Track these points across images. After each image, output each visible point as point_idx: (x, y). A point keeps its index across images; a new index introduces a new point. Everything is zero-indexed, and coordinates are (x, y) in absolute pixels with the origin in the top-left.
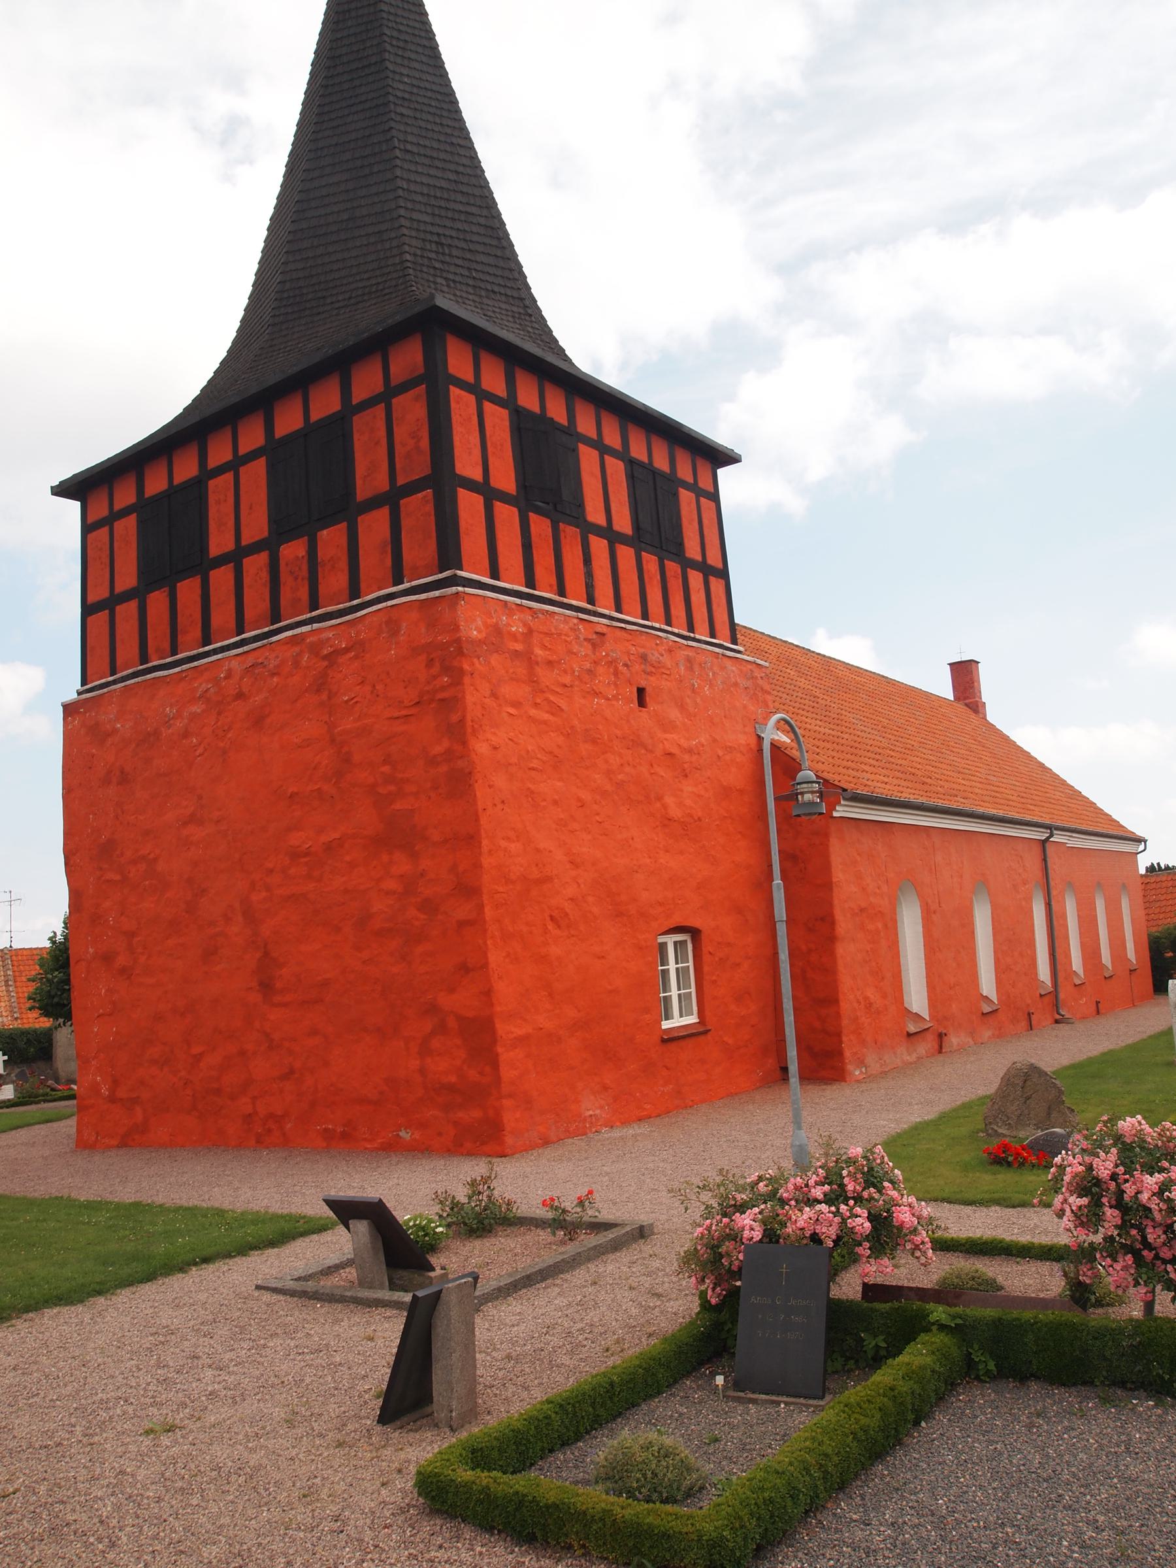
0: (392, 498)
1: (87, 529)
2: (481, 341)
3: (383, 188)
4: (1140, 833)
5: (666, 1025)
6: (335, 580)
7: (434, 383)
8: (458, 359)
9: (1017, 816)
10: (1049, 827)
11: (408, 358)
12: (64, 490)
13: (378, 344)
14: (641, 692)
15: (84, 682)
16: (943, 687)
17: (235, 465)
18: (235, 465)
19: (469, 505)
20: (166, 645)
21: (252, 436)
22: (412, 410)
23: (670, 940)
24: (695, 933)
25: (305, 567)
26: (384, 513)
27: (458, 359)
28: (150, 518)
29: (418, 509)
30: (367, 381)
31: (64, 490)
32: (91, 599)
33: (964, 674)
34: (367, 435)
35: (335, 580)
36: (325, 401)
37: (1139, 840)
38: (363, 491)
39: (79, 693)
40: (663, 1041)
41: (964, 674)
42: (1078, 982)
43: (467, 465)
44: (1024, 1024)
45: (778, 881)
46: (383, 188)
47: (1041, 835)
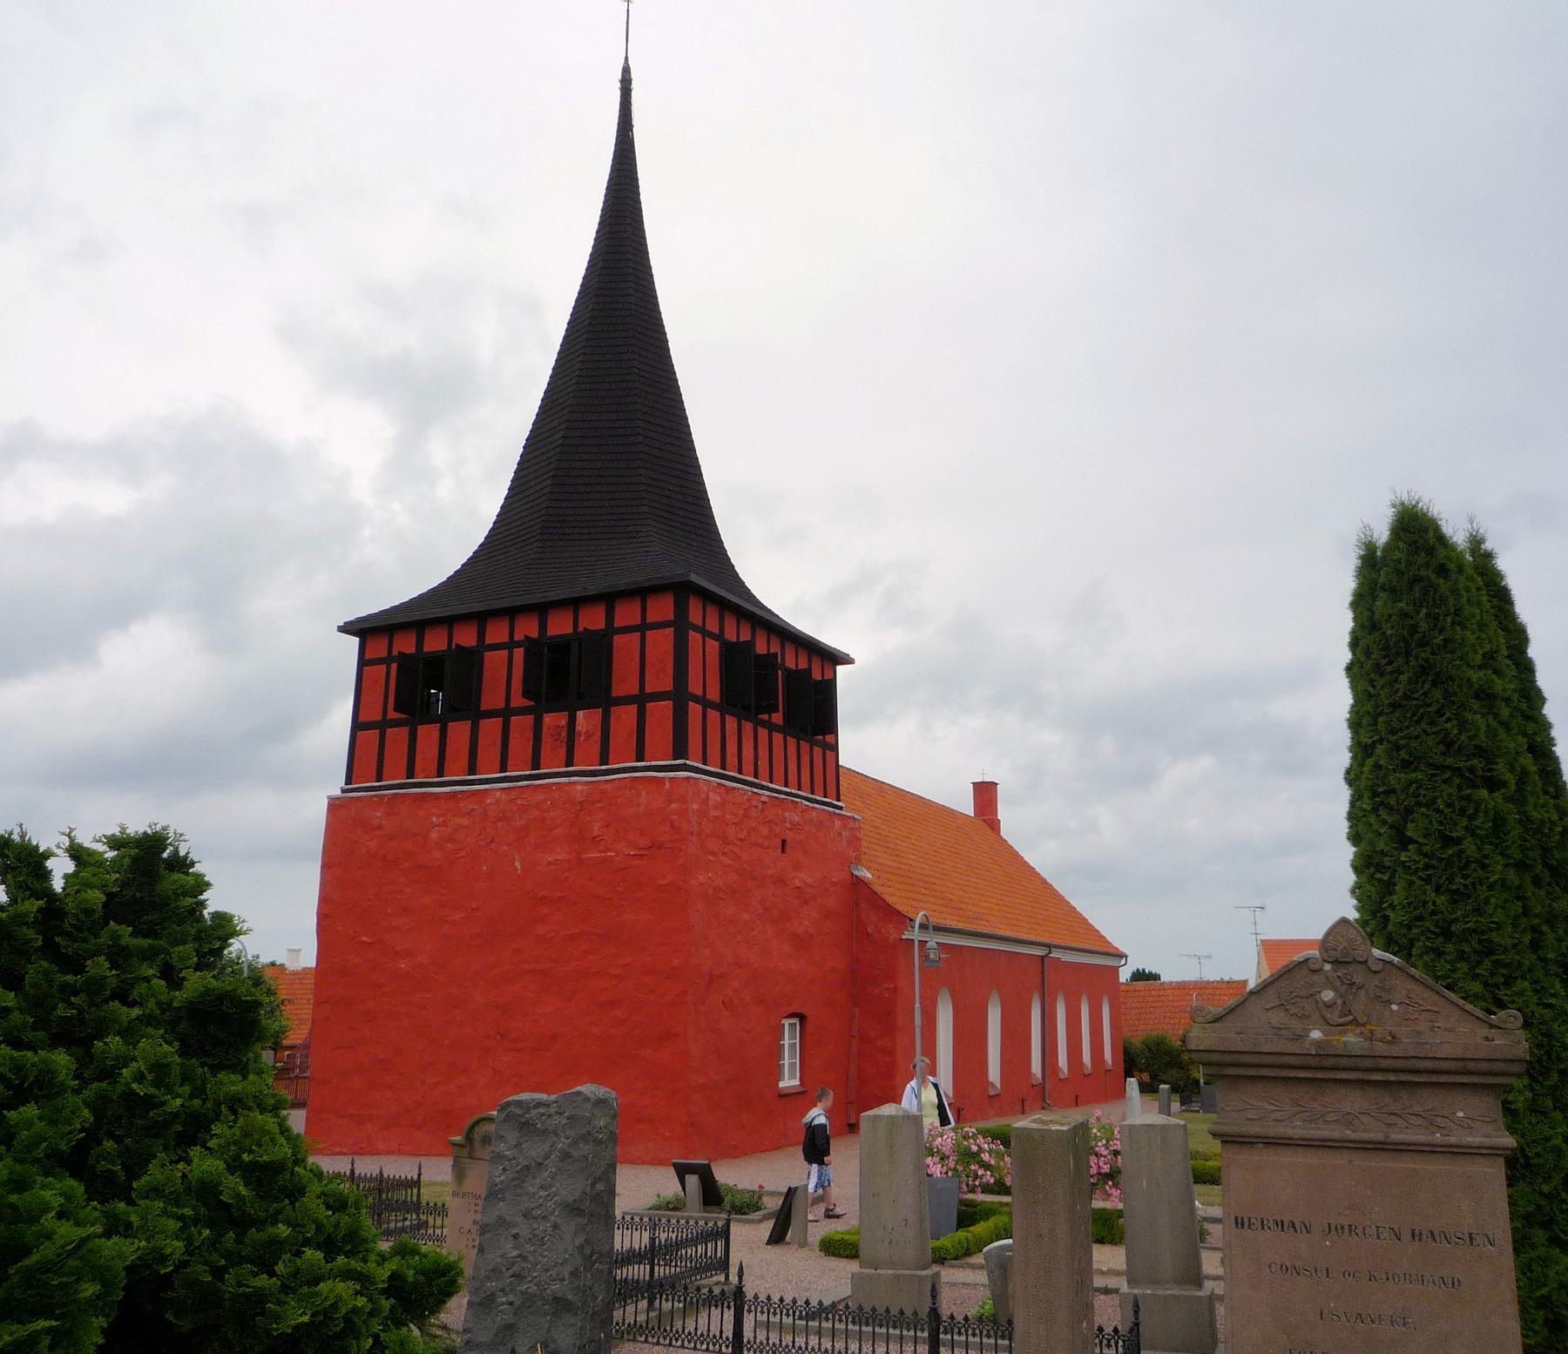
0: (642, 699)
1: (363, 662)
2: (708, 597)
3: (614, 395)
4: (1123, 949)
5: (781, 1085)
6: (587, 747)
7: (680, 625)
8: (695, 613)
9: (1025, 937)
10: (1049, 946)
11: (661, 608)
12: (346, 629)
13: (642, 593)
14: (784, 842)
15: (349, 781)
16: (967, 807)
17: (643, 628)
18: (510, 645)
19: (694, 709)
20: (434, 767)
21: (527, 628)
22: (661, 643)
23: (786, 1022)
24: (802, 1018)
25: (564, 734)
26: (634, 708)
27: (695, 613)
28: (418, 668)
29: (660, 713)
30: (627, 614)
31: (346, 629)
32: (363, 718)
33: (985, 793)
34: (625, 648)
35: (587, 747)
36: (593, 619)
37: (1121, 956)
38: (617, 691)
39: (343, 791)
40: (781, 1096)
41: (985, 793)
42: (992, 1093)
43: (695, 687)
44: (1019, 1107)
45: (917, 1005)
46: (614, 395)
47: (1040, 952)
